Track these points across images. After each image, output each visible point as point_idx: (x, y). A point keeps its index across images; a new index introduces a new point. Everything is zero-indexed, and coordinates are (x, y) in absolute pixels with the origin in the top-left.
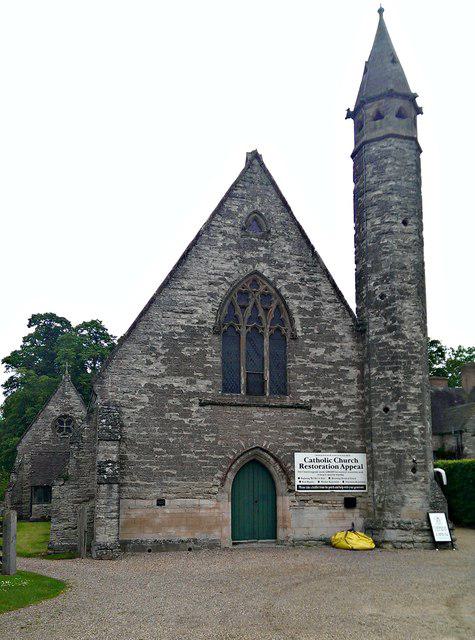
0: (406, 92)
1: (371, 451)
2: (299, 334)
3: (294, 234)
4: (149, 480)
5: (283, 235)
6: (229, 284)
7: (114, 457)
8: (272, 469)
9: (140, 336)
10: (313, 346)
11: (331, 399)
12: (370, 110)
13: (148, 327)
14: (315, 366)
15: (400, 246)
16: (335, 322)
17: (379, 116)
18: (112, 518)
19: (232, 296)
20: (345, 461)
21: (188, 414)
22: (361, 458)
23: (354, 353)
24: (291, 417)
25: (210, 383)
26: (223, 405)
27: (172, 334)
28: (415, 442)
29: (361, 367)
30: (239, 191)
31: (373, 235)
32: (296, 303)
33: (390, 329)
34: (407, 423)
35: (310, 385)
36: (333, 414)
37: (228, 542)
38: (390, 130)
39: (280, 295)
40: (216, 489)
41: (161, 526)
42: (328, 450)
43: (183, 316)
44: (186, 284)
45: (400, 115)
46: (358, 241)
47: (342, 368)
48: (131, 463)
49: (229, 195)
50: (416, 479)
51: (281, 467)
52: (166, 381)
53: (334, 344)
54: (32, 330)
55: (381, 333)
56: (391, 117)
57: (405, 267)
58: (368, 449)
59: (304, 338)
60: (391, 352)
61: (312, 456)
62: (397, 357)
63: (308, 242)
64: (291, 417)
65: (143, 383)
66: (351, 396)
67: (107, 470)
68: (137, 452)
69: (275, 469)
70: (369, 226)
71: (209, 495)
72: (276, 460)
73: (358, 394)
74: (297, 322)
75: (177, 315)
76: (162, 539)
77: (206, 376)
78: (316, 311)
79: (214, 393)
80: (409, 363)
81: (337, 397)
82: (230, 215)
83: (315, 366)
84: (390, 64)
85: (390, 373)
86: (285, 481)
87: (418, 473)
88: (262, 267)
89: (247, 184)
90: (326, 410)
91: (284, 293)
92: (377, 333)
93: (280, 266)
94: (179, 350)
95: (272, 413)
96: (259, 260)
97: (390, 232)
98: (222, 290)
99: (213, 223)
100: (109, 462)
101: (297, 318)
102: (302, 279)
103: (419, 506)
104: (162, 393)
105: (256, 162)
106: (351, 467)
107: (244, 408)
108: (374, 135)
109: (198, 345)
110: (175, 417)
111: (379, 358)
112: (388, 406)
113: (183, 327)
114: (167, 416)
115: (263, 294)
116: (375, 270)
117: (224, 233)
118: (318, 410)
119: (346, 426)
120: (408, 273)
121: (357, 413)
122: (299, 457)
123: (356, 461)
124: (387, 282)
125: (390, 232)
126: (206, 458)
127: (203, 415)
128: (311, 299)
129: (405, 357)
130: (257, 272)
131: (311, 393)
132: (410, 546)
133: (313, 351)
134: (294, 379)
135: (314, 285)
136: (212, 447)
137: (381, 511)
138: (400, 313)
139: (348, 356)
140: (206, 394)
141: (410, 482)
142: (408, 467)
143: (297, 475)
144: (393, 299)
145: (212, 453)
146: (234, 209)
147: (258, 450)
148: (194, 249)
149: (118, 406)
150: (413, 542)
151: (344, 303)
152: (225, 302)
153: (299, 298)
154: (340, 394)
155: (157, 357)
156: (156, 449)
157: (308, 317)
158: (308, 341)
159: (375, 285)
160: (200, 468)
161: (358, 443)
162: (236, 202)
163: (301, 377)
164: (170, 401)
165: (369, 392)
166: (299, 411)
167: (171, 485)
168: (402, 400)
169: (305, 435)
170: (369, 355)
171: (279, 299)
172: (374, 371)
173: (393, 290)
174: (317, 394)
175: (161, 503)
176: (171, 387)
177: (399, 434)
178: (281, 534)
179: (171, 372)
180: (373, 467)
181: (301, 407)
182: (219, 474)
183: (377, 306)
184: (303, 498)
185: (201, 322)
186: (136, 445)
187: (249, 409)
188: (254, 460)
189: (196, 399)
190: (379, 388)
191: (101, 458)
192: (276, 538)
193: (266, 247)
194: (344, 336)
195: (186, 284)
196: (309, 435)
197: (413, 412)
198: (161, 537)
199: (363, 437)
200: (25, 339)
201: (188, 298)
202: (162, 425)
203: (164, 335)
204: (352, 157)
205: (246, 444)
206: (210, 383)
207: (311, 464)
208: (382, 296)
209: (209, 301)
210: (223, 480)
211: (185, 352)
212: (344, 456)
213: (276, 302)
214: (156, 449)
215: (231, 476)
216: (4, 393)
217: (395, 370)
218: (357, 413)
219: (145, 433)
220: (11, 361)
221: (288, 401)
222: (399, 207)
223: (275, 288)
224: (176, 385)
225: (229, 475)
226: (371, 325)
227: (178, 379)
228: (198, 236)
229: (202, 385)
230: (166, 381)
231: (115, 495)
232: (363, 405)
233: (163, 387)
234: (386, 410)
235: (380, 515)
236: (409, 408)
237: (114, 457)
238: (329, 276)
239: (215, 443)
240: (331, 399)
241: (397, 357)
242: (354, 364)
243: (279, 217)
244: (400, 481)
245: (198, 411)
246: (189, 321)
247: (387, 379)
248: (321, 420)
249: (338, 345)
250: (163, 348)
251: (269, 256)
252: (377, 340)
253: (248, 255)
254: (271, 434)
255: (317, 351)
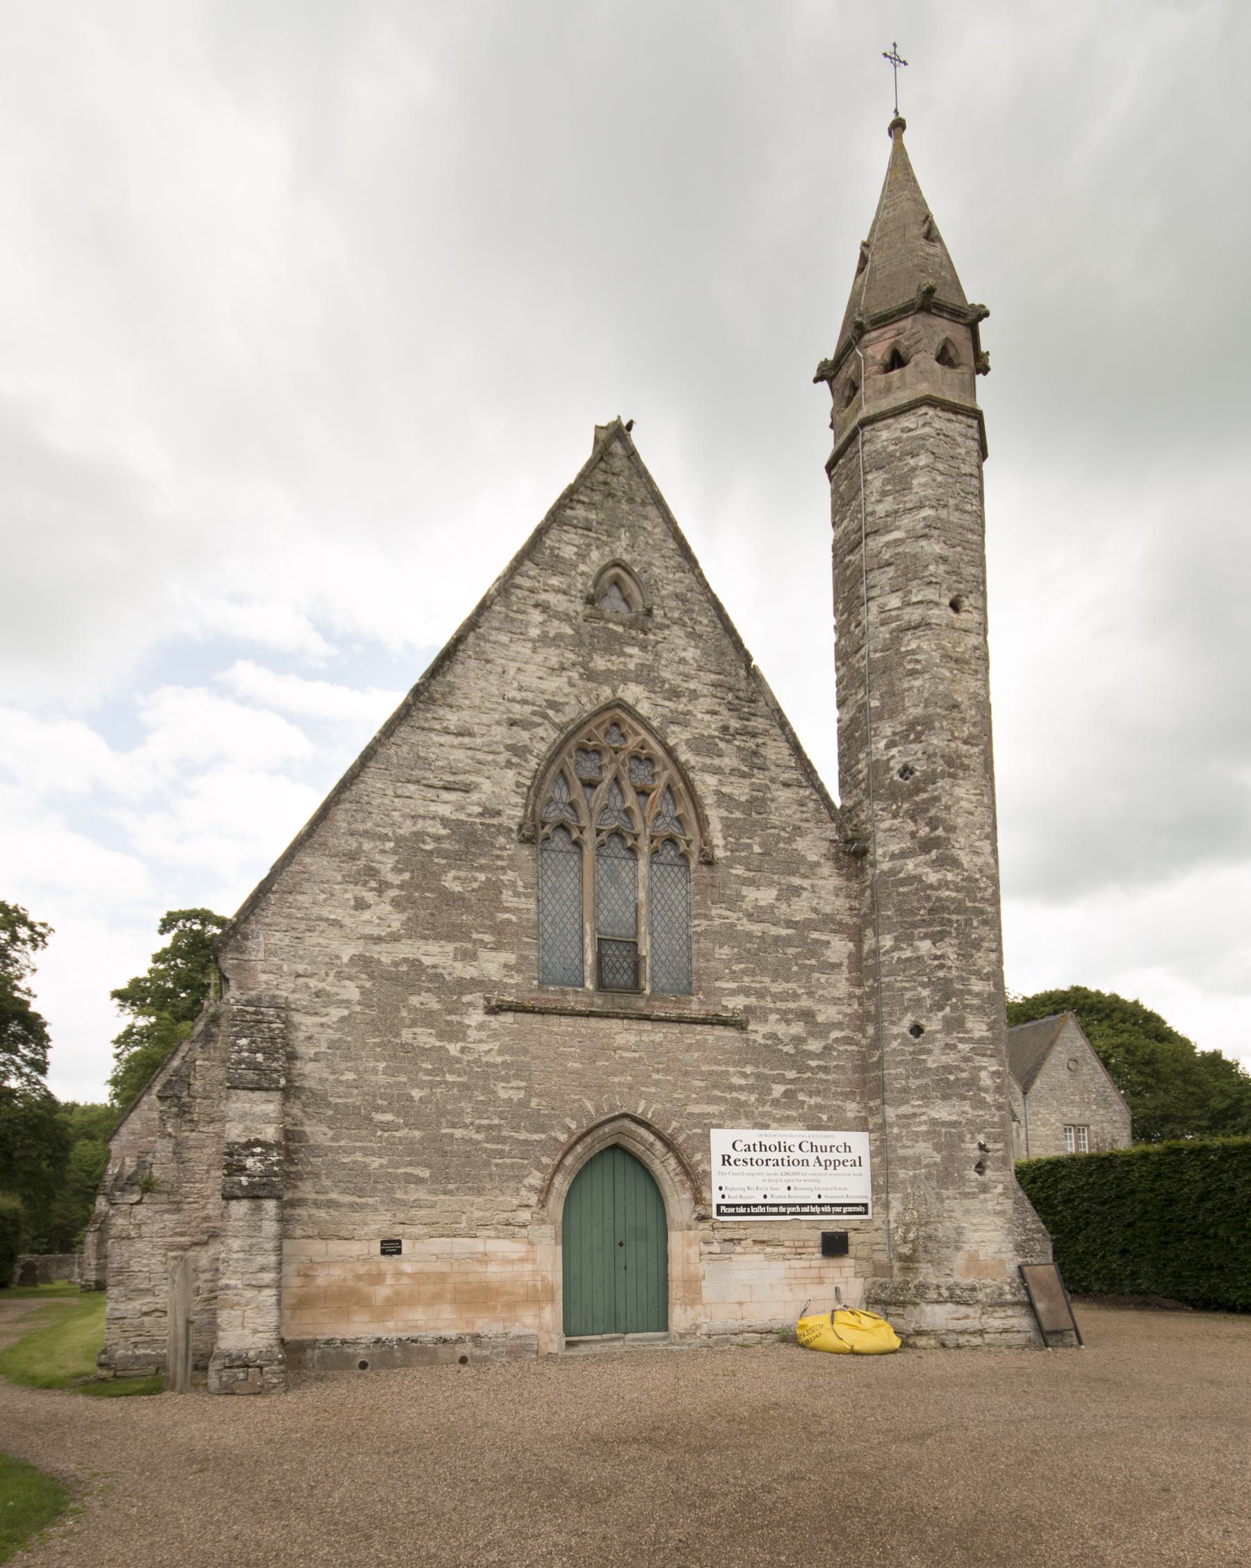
0: (957, 302)
1: (882, 1126)
2: (720, 853)
3: (704, 623)
4: (360, 1192)
5: (680, 622)
6: (554, 725)
7: (270, 1133)
8: (657, 1167)
9: (339, 835)
10: (751, 882)
11: (792, 1005)
12: (877, 347)
13: (359, 816)
14: (756, 928)
15: (946, 657)
16: (798, 831)
17: (897, 360)
18: (260, 1287)
19: (564, 755)
20: (824, 1149)
21: (456, 1032)
22: (860, 1142)
23: (841, 903)
24: (701, 1046)
25: (512, 958)
26: (542, 1012)
27: (419, 836)
28: (981, 1104)
29: (857, 936)
30: (580, 512)
31: (884, 633)
32: (712, 780)
33: (926, 846)
34: (966, 1059)
35: (745, 972)
36: (797, 1040)
37: (554, 1342)
38: (924, 389)
39: (675, 761)
40: (524, 1215)
41: (395, 1302)
42: (784, 1121)
43: (446, 796)
44: (452, 719)
45: (945, 357)
46: (842, 656)
47: (815, 935)
48: (314, 1150)
49: (556, 516)
50: (984, 1188)
51: (680, 1162)
52: (405, 950)
53: (797, 881)
54: (167, 941)
55: (904, 855)
56: (924, 360)
57: (955, 706)
58: (872, 1121)
59: (732, 861)
60: (928, 898)
61: (751, 1136)
62: (944, 909)
63: (738, 644)
64: (701, 1046)
65: (347, 952)
66: (836, 1001)
67: (249, 1162)
68: (331, 1122)
69: (665, 1168)
70: (871, 614)
71: (509, 1228)
72: (669, 1144)
73: (851, 996)
74: (715, 828)
75: (431, 794)
76: (393, 1335)
77: (502, 936)
78: (757, 804)
79: (517, 986)
80: (968, 922)
81: (805, 1003)
82: (556, 565)
83: (756, 928)
84: (923, 242)
85: (925, 946)
86: (688, 1195)
87: (988, 1173)
88: (632, 693)
89: (597, 498)
90: (781, 1030)
91: (685, 755)
92: (893, 857)
93: (675, 694)
94: (437, 876)
95: (656, 1034)
96: (625, 678)
97: (924, 624)
98: (543, 739)
99: (518, 580)
100: (258, 1143)
101: (715, 816)
102: (725, 729)
103: (992, 1248)
104: (395, 979)
105: (617, 447)
106: (836, 1164)
107: (593, 1022)
108: (886, 404)
109: (481, 868)
110: (425, 1037)
111: (900, 911)
112: (923, 1022)
113: (445, 822)
114: (406, 1035)
115: (636, 757)
116: (891, 710)
117: (543, 607)
118: (763, 1029)
119: (825, 1069)
120: (963, 720)
121: (848, 1041)
122: (721, 1140)
123: (847, 1148)
124: (918, 740)
125: (924, 624)
126: (504, 1140)
127: (495, 1036)
128: (744, 775)
129: (957, 911)
130: (620, 704)
131: (746, 992)
132: (976, 1341)
133: (751, 894)
134: (708, 956)
135: (751, 744)
136: (518, 1113)
137: (908, 1262)
138: (948, 808)
139: (828, 910)
140: (496, 985)
141: (973, 1195)
142: (968, 1160)
143: (716, 1181)
144: (931, 778)
145: (517, 1128)
146: (568, 552)
147: (627, 1123)
148: (471, 638)
149: (283, 1008)
150: (982, 1332)
151: (819, 788)
152: (547, 768)
153: (717, 771)
154: (810, 994)
155: (380, 891)
156: (379, 1117)
157: (738, 815)
158: (739, 871)
159: (891, 745)
160: (487, 1164)
161: (852, 1109)
162: (572, 536)
163: (725, 952)
164: (414, 1000)
165: (875, 991)
166: (719, 1031)
167: (417, 1204)
168: (954, 1008)
169: (732, 1088)
170: (875, 906)
171: (672, 771)
172: (887, 941)
173: (930, 757)
174: (761, 994)
175: (391, 1247)
176: (416, 965)
177: (948, 1084)
178: (679, 1318)
179: (416, 930)
180: (887, 1162)
181: (725, 1023)
182: (535, 1179)
183: (894, 794)
184: (729, 1235)
185: (489, 812)
186: (329, 1104)
187: (604, 1024)
188: (615, 1147)
189: (476, 998)
190: (899, 981)
191: (235, 1133)
192: (666, 1328)
193: (643, 647)
194: (818, 864)
195: (452, 719)
196: (741, 1088)
197: (977, 1034)
198: (390, 1329)
199: (862, 1094)
200: (157, 958)
201: (460, 754)
202: (394, 1057)
203: (398, 840)
204: (830, 467)
205: (598, 1109)
206: (512, 958)
207: (748, 1155)
208: (906, 771)
209: (509, 765)
210: (545, 1192)
211: (451, 882)
212: (821, 1138)
213: (665, 775)
214: (379, 1117)
215: (562, 1184)
216: (117, 1056)
217: (937, 938)
218: (848, 1041)
219: (350, 1076)
220: (131, 996)
221: (695, 1007)
222: (942, 568)
223: (663, 744)
224: (427, 961)
225: (558, 1180)
226: (880, 836)
227: (433, 947)
228: (484, 607)
229: (492, 964)
230: (405, 950)
231: (270, 1227)
232: (861, 1021)
233: (396, 964)
234: (917, 1030)
235: (905, 1270)
236: (969, 1025)
237: (270, 1133)
238: (784, 724)
239: (524, 1103)
240: (792, 1005)
241: (944, 909)
242: (840, 928)
243: (671, 582)
244: (951, 1192)
245: (481, 1027)
246: (461, 808)
247: (919, 959)
248: (770, 1053)
249: (806, 883)
250: (396, 870)
251: (651, 668)
252: (893, 872)
253: (600, 663)
254: (657, 1083)
255: (758, 894)
